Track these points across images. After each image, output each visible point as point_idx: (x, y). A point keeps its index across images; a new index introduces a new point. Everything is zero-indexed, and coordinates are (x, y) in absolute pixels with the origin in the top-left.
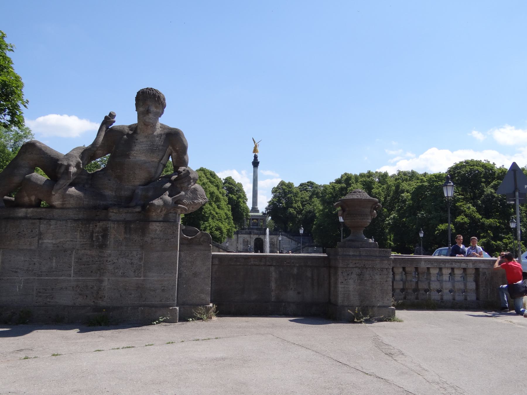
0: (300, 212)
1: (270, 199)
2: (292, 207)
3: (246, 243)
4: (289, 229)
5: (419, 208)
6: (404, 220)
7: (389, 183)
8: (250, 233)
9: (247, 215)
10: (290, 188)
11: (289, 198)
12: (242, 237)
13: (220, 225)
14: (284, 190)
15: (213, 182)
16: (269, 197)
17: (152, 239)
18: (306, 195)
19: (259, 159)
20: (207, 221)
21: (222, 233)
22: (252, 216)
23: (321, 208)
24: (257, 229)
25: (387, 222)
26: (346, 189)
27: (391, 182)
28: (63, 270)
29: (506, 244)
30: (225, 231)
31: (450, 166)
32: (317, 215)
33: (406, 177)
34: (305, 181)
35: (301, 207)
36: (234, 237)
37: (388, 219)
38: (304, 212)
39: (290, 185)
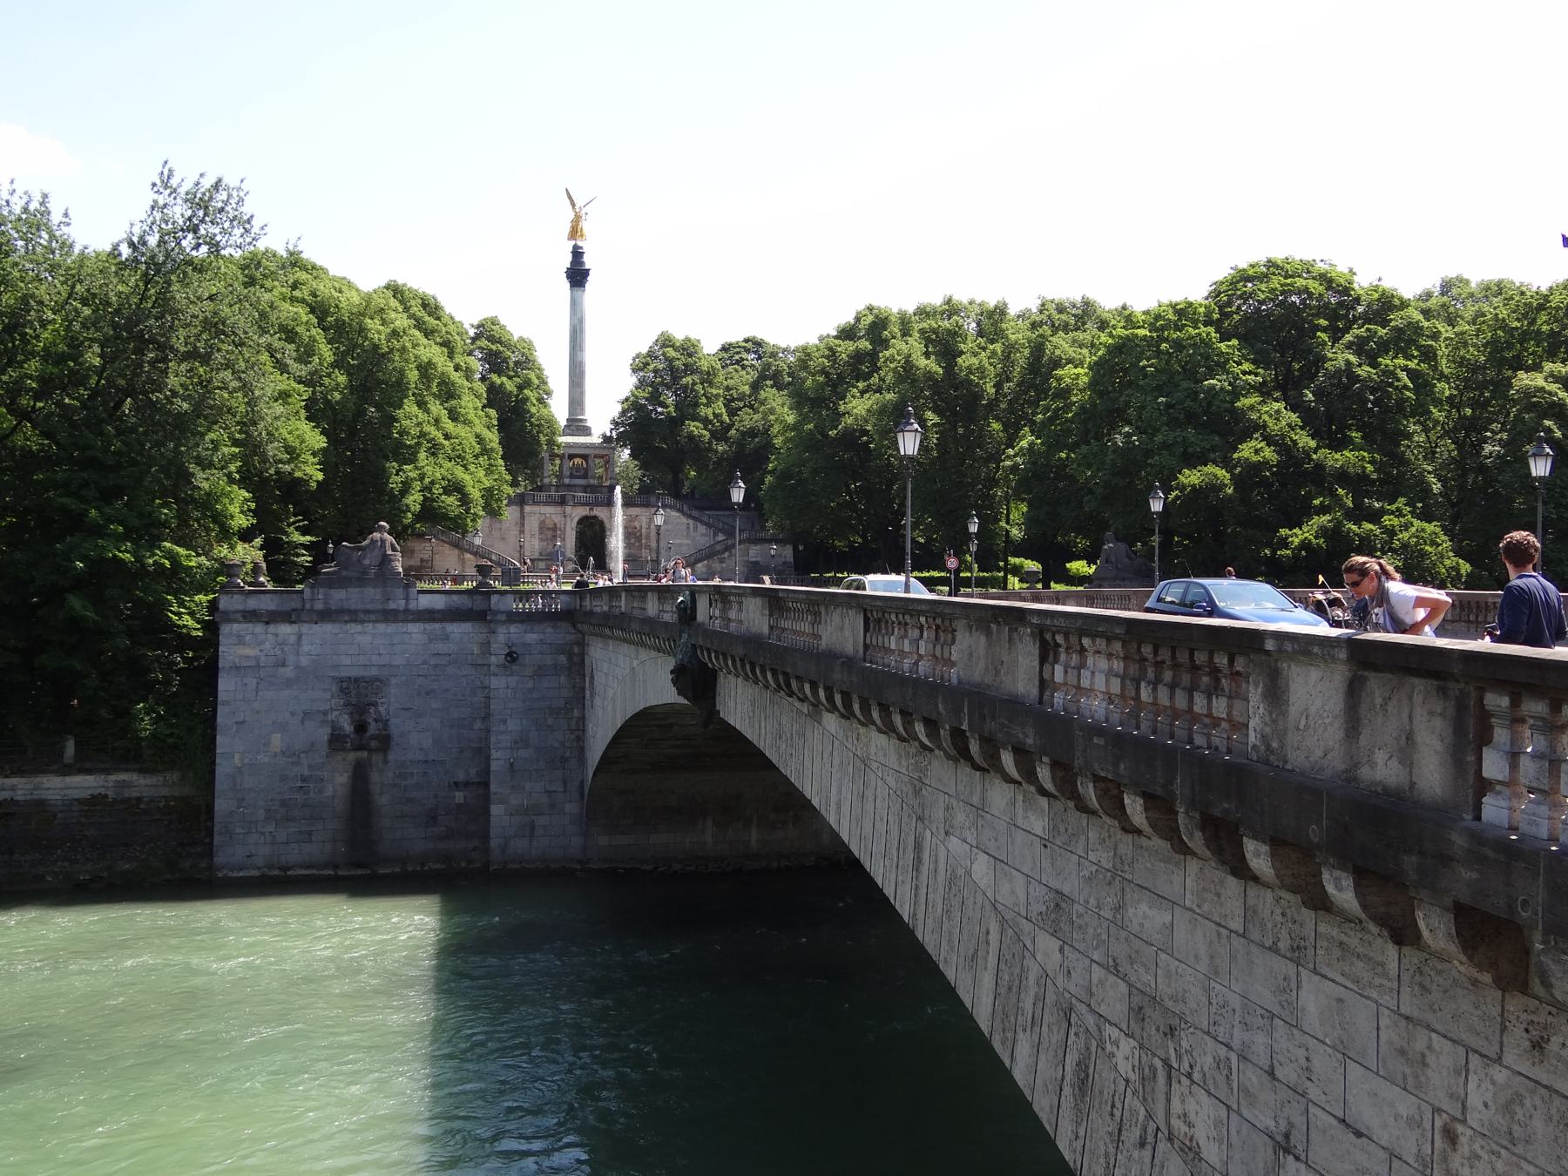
0: (720, 434)
1: (625, 393)
2: (695, 418)
3: (550, 532)
4: (685, 490)
5: (1116, 416)
6: (1063, 455)
7: (1013, 337)
8: (562, 502)
9: (551, 443)
10: (690, 355)
11: (686, 387)
12: (537, 513)
13: (459, 473)
14: (670, 361)
15: (432, 332)
18: (742, 381)
19: (588, 261)
20: (412, 460)
21: (465, 500)
22: (568, 445)
23: (791, 419)
24: (585, 489)
25: (1008, 463)
26: (873, 356)
27: (1018, 334)
29: (1391, 532)
30: (475, 494)
31: (1220, 277)
32: (778, 441)
33: (1064, 317)
34: (736, 337)
35: (726, 418)
36: (509, 514)
37: (1011, 452)
38: (733, 432)
39: (689, 349)
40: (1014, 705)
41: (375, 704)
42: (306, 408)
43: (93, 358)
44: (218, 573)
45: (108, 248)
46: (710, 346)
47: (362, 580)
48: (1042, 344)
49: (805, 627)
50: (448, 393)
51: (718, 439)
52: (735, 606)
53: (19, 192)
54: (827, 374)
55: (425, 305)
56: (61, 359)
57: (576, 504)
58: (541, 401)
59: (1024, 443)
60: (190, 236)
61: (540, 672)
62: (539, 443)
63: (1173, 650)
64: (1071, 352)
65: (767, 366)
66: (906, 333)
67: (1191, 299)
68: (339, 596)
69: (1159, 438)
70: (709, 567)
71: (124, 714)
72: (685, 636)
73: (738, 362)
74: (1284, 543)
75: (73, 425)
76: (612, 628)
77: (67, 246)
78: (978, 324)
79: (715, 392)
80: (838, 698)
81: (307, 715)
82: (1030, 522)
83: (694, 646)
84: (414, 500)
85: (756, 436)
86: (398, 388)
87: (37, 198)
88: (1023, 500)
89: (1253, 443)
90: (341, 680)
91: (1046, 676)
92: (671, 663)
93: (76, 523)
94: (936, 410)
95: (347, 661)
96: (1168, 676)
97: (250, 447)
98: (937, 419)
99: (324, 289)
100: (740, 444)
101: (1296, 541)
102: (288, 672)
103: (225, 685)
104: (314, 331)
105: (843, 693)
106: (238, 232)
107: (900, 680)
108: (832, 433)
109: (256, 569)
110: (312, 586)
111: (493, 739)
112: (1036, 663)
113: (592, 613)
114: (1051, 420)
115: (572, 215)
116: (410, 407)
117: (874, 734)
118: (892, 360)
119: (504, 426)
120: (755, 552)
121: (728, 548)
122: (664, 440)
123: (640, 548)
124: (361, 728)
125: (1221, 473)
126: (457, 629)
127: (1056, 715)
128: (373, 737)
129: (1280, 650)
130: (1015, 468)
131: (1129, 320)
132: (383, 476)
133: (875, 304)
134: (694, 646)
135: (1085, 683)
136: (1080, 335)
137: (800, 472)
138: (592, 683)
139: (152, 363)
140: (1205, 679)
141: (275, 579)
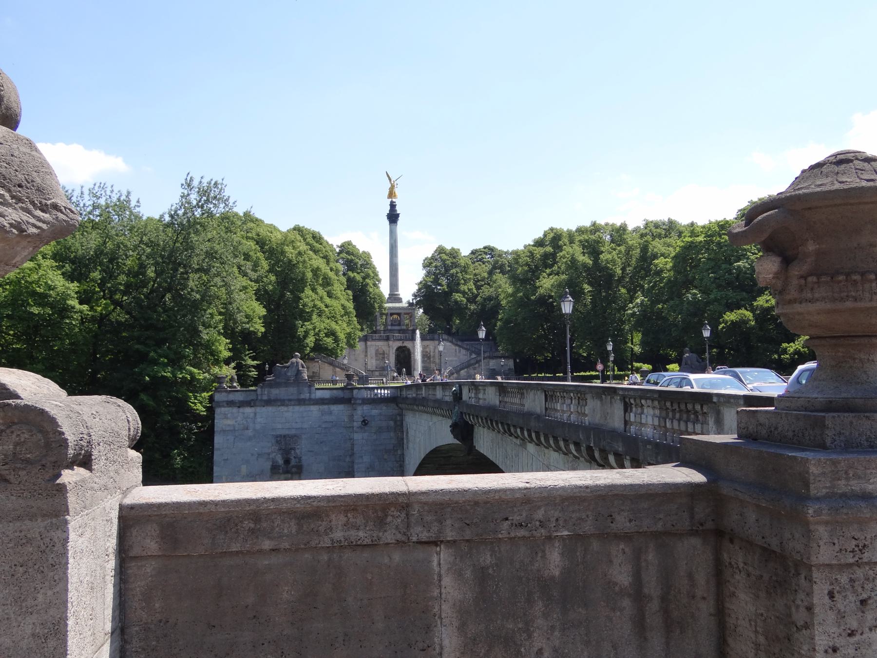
0: (472, 299)
2: (458, 291)
4: (454, 330)
5: (688, 284)
6: (660, 306)
7: (630, 243)
8: (387, 339)
9: (381, 307)
10: (454, 258)
12: (374, 345)
13: (334, 326)
14: (444, 261)
18: (483, 270)
19: (399, 209)
21: (337, 340)
22: (390, 308)
24: (399, 331)
26: (554, 255)
27: (633, 241)
30: (342, 336)
32: (504, 303)
33: (658, 230)
34: (480, 246)
35: (475, 291)
36: (360, 346)
37: (631, 305)
38: (479, 298)
39: (454, 254)
40: (613, 433)
41: (294, 449)
42: (256, 294)
43: (151, 273)
44: (213, 381)
45: (157, 217)
46: (465, 252)
47: (287, 384)
48: (647, 246)
49: (517, 400)
50: (327, 282)
51: (471, 303)
52: (482, 391)
53: (116, 191)
54: (529, 265)
55: (314, 238)
56: (136, 275)
57: (394, 340)
58: (375, 285)
59: (638, 301)
60: (199, 210)
61: (380, 430)
62: (374, 308)
63: (679, 403)
64: (663, 250)
65: (496, 262)
66: (572, 242)
67: (728, 219)
68: (275, 392)
69: (712, 296)
70: (468, 372)
71: (168, 456)
72: (457, 408)
73: (480, 260)
74: (785, 351)
75: (141, 307)
76: (417, 405)
77: (138, 217)
78: (611, 236)
79: (468, 277)
80: (533, 435)
81: (260, 455)
82: (643, 343)
83: (461, 413)
84: (310, 341)
85: (491, 300)
86: (303, 281)
87: (125, 193)
88: (639, 331)
89: (765, 297)
90: (277, 436)
91: (627, 419)
92: (450, 422)
93: (143, 358)
94: (590, 284)
95: (279, 426)
96: (677, 416)
97: (228, 316)
98: (590, 289)
99: (263, 232)
100: (483, 305)
101: (792, 350)
102: (250, 433)
103: (218, 440)
104: (258, 254)
105: (536, 432)
106: (222, 205)
107: (562, 424)
108: (533, 298)
109: (232, 380)
110: (262, 388)
111: (356, 466)
112: (623, 413)
113: (407, 398)
114: (653, 287)
116: (308, 291)
117: (552, 453)
118: (564, 257)
119: (355, 299)
120: (493, 364)
121: (478, 362)
122: (441, 304)
123: (430, 363)
124: (287, 462)
125: (749, 314)
126: (336, 408)
127: (631, 437)
128: (293, 467)
129: (719, 401)
130: (634, 314)
131: (693, 234)
132: (294, 328)
133: (554, 226)
134: (461, 413)
135: (643, 421)
136: (668, 240)
137: (516, 319)
138: (407, 435)
139: (182, 273)
140: (692, 416)
141: (242, 385)
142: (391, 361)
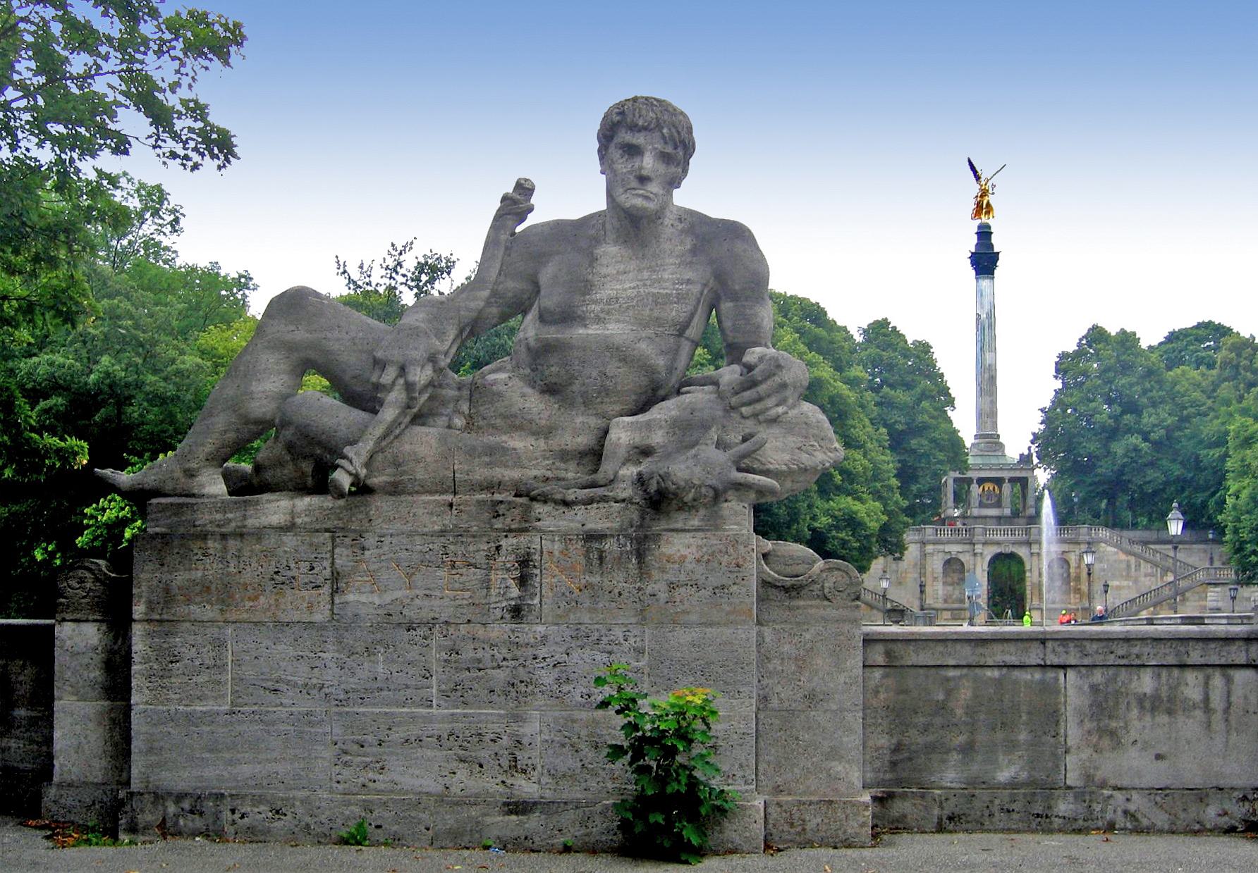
16: (1046, 387)
17: (672, 586)
28: (407, 687)
39: (1127, 340)
115: (975, 189)
142: (979, 583)
